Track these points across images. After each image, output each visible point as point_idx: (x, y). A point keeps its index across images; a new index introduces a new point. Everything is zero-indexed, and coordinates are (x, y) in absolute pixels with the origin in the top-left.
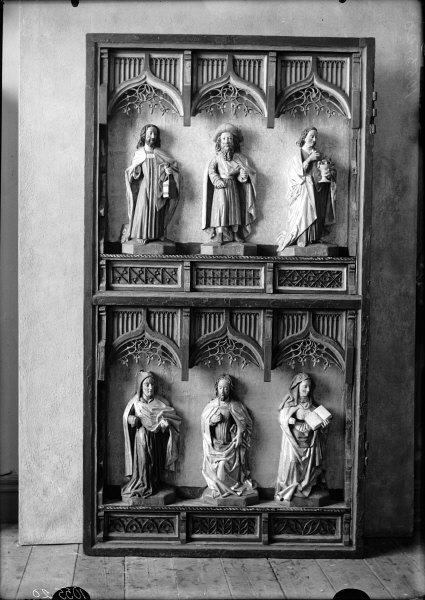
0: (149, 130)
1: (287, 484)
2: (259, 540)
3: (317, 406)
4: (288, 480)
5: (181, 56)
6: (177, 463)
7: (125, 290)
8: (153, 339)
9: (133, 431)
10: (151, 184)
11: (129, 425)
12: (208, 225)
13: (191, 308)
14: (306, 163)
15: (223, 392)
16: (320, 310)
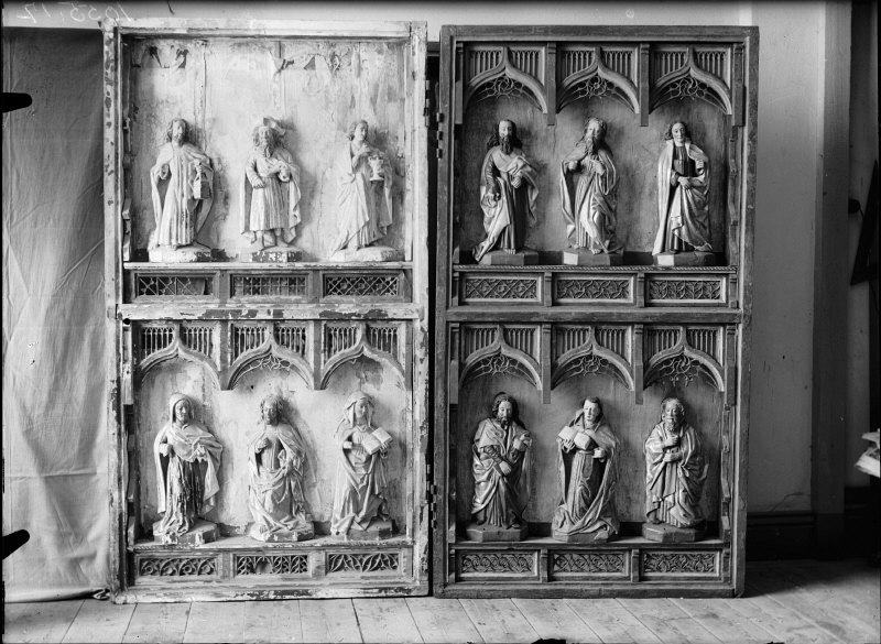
0: (176, 125)
1: (343, 516)
2: (628, 578)
3: (376, 428)
4: (343, 511)
6: (218, 496)
7: (479, 305)
9: (165, 461)
10: (180, 184)
11: (161, 455)
12: (247, 229)
13: (645, 324)
14: (355, 159)
15: (269, 414)
16: (604, 323)
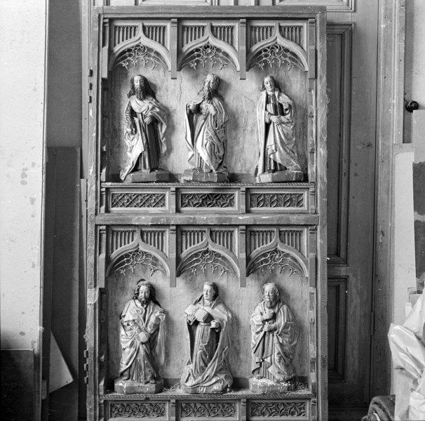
5: (236, 25)
8: (146, 251)
